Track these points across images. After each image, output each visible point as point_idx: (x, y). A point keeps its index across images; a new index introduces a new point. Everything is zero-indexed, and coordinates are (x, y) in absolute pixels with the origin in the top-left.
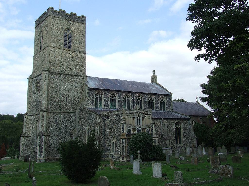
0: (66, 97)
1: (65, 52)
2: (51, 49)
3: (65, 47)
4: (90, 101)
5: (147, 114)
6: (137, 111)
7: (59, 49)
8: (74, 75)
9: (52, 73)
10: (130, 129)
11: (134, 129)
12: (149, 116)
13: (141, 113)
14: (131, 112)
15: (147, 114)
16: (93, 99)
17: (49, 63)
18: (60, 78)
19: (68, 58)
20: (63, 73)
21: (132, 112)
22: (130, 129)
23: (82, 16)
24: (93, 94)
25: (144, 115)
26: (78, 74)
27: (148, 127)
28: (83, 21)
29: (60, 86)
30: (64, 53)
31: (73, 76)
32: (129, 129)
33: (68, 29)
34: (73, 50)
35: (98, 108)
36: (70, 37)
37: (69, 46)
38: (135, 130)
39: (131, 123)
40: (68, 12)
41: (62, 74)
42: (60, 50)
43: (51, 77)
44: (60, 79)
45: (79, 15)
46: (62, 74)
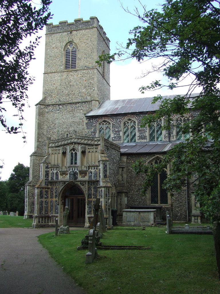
0: (67, 134)
1: (66, 75)
3: (67, 67)
5: (92, 145)
6: (72, 141)
7: (58, 73)
8: (78, 103)
9: (49, 105)
10: (57, 173)
11: (63, 173)
13: (79, 144)
14: (60, 144)
15: (92, 145)
17: (45, 94)
18: (58, 110)
19: (70, 82)
21: (63, 143)
22: (57, 173)
23: (92, 18)
24: (95, 125)
25: (85, 148)
26: (83, 100)
28: (91, 25)
30: (65, 76)
31: (76, 104)
32: (55, 172)
33: (70, 43)
34: (78, 69)
35: (155, 141)
36: (74, 52)
38: (67, 174)
40: (71, 21)
41: (60, 104)
42: (60, 74)
43: (47, 111)
44: (58, 111)
45: (86, 18)
46: (60, 104)
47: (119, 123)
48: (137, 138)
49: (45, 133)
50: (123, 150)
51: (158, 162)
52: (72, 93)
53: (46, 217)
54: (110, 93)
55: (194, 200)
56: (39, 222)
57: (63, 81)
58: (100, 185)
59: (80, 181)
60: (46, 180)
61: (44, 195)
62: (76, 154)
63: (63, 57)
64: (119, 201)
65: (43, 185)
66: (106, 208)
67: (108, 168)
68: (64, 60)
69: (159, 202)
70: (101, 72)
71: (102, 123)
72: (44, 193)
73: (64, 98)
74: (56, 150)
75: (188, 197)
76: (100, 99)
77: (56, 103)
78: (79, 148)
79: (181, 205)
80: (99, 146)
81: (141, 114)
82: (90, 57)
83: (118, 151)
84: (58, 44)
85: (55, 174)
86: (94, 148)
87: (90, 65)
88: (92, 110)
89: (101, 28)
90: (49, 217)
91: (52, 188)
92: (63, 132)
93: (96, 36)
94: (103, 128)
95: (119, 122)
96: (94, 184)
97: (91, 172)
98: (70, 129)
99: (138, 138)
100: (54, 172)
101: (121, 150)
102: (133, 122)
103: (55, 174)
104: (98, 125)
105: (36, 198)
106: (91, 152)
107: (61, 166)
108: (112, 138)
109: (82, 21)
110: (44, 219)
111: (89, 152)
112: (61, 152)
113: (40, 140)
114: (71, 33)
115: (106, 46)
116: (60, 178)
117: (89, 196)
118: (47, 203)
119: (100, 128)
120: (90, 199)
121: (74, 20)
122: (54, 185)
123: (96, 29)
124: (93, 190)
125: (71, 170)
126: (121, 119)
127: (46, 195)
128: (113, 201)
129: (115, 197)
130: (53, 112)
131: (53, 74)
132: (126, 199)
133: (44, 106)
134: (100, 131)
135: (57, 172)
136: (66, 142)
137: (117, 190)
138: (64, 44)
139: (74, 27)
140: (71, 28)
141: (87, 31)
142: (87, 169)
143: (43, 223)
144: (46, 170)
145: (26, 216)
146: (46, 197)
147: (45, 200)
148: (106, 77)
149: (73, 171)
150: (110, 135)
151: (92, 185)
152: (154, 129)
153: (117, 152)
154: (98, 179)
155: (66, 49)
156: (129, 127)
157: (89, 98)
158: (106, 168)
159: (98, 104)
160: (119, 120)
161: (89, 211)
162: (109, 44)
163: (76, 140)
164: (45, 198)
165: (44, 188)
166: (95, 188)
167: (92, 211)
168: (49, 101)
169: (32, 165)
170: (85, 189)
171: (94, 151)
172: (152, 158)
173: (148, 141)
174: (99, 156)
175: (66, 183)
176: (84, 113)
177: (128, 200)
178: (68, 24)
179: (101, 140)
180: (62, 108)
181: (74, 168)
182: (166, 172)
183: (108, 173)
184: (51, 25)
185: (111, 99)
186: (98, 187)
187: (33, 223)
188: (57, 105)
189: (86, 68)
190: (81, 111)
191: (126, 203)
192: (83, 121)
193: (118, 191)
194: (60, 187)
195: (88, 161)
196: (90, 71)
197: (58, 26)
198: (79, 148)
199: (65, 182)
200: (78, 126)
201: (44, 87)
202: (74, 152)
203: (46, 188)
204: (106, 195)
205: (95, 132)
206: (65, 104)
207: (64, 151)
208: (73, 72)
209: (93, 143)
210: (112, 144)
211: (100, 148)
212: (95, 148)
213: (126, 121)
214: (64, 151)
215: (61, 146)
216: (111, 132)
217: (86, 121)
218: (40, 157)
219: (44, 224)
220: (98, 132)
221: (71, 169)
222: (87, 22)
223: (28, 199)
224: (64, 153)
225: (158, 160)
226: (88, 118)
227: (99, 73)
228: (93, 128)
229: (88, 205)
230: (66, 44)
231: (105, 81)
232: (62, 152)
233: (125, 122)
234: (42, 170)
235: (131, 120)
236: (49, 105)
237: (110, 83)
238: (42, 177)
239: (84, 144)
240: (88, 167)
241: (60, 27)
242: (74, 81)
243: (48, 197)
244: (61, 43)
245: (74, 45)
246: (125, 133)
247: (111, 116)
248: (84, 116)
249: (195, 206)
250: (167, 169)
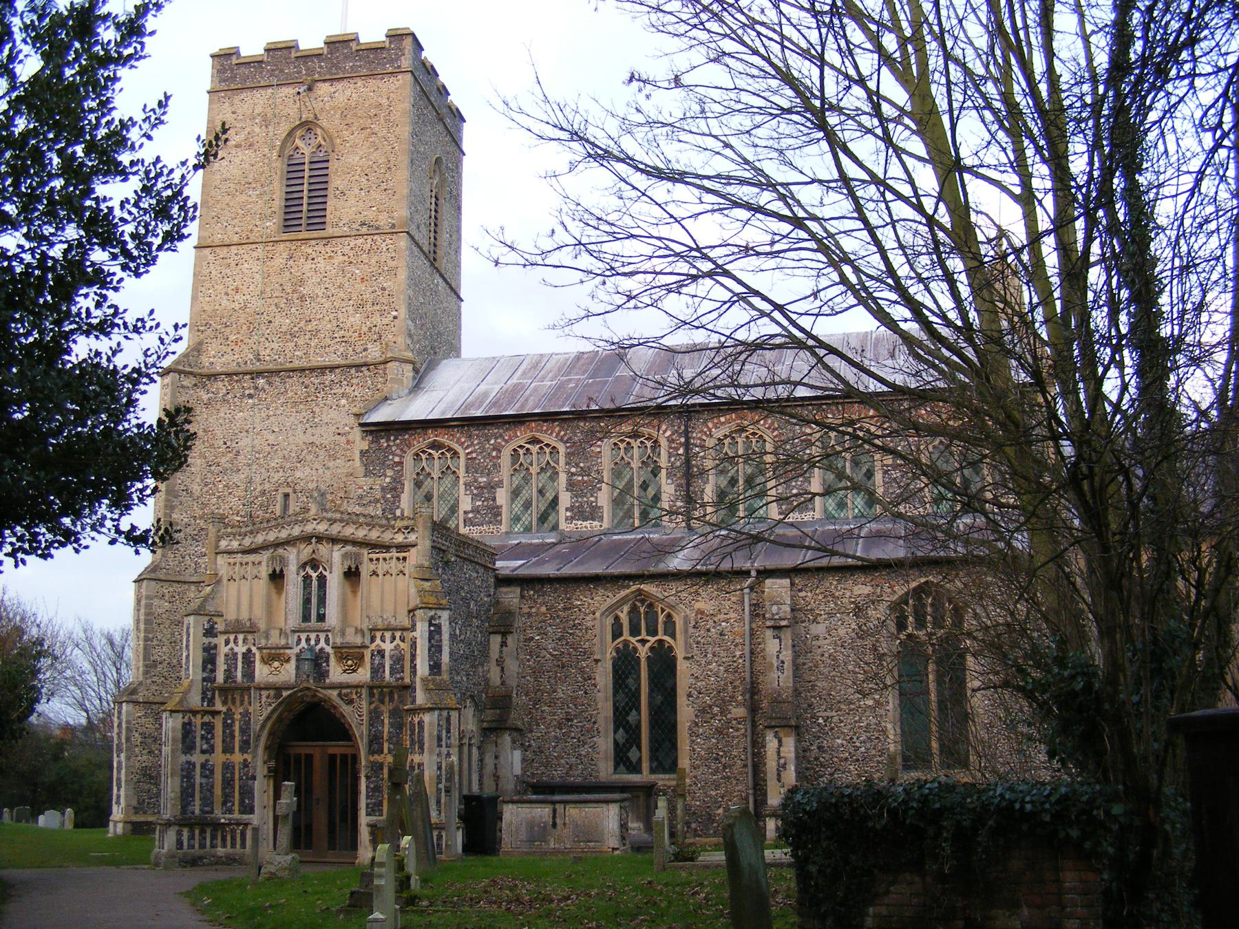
0: (287, 496)
1: (285, 255)
2: (211, 257)
3: (289, 223)
4: (377, 501)
5: (387, 548)
6: (309, 528)
8: (332, 368)
10: (248, 657)
11: (274, 656)
12: (401, 555)
13: (334, 540)
14: (260, 539)
15: (387, 548)
16: (395, 489)
18: (251, 396)
19: (302, 282)
20: (271, 367)
21: (272, 536)
22: (248, 657)
23: (397, 36)
24: (397, 459)
25: (357, 557)
27: (241, 637)
28: (391, 61)
29: (249, 440)
31: (323, 374)
32: (241, 649)
33: (308, 126)
36: (321, 166)
37: (316, 214)
38: (288, 661)
39: (259, 613)
40: (311, 41)
42: (260, 251)
43: (205, 397)
45: (372, 33)
46: (260, 374)
47: (494, 454)
48: (563, 513)
49: (196, 488)
50: (505, 566)
51: (642, 610)
52: (309, 328)
53: (208, 825)
54: (459, 328)
55: (776, 757)
56: (180, 844)
57: (273, 279)
58: (414, 701)
59: (340, 686)
60: (204, 680)
61: (198, 739)
62: (322, 580)
63: (276, 184)
64: (489, 760)
65: (195, 700)
66: (439, 790)
67: (446, 636)
68: (278, 191)
69: (645, 765)
70: (427, 243)
71: (424, 452)
72: (199, 732)
73: (275, 346)
74: (247, 564)
75: (754, 743)
76: (420, 352)
77: (243, 368)
78: (336, 558)
79: (729, 778)
80: (413, 550)
81: (579, 419)
82: (384, 186)
83: (486, 567)
84: (257, 130)
85: (240, 657)
86: (391, 558)
87: (384, 221)
88: (386, 399)
89: (431, 72)
90: (216, 826)
91: (229, 714)
92: (267, 486)
93: (407, 105)
94: (429, 474)
95: (494, 449)
96: (392, 700)
97: (381, 653)
98: (298, 474)
99: (569, 514)
100: (236, 649)
101: (499, 564)
102: (547, 450)
103: (240, 657)
104: (409, 459)
105: (167, 750)
106: (380, 572)
107: (262, 626)
108: (465, 512)
109: (354, 46)
110: (197, 832)
111: (375, 573)
112: (264, 571)
113: (174, 516)
114: (310, 89)
115: (448, 138)
116: (262, 672)
117: (375, 743)
118: (207, 770)
119: (418, 474)
120: (376, 757)
121: (324, 38)
122: (238, 702)
123: (409, 77)
124: (386, 721)
125: (303, 644)
126: (501, 436)
127: (207, 739)
128: (466, 765)
129: (475, 751)
130: (228, 401)
131: (234, 249)
132: (517, 755)
133: (192, 380)
134: (418, 484)
135: (249, 650)
136: (284, 534)
137: (483, 721)
138: (284, 129)
139: (321, 67)
140: (310, 71)
141: (373, 83)
142: (367, 642)
143: (193, 847)
144: (206, 640)
145: (120, 826)
146: (205, 747)
147: (203, 758)
148: (443, 264)
149: (311, 649)
150: (457, 500)
151: (382, 702)
152: (631, 479)
153: (481, 570)
154: (407, 681)
155: (288, 152)
156: (534, 470)
157: (374, 353)
158: (437, 637)
159: (411, 374)
160: (492, 442)
161: (375, 804)
162: (460, 130)
163: (322, 528)
164: (203, 752)
165: (197, 712)
166: (394, 713)
167: (385, 803)
168: (216, 358)
169: (142, 618)
170: (356, 716)
171: (394, 571)
172: (619, 596)
173: (606, 524)
174: (413, 591)
175: (285, 694)
176: (355, 410)
177: (524, 760)
178: (299, 54)
179: (420, 529)
180: (267, 387)
181: (313, 636)
182: (671, 648)
183: (445, 658)
184: (234, 57)
185: (466, 351)
186: (407, 710)
187: (157, 850)
188: (248, 377)
189: (364, 230)
190: (343, 401)
191: (518, 770)
192: (348, 442)
193: (485, 725)
194: (260, 710)
195: (368, 607)
196: (383, 243)
197: (261, 62)
198: (336, 558)
199: (278, 689)
200: (331, 464)
201: (194, 298)
202: (314, 575)
203: (205, 713)
204: (439, 739)
205: (395, 489)
206: (277, 372)
207: (278, 570)
208: (313, 242)
209: (387, 537)
210: (464, 543)
211: (414, 556)
212: (398, 559)
213: (521, 447)
214: (278, 570)
215: (264, 547)
216: (462, 488)
217: (361, 443)
218: (175, 585)
219: (197, 850)
220: (408, 486)
221: (303, 636)
222: (375, 49)
223: (128, 758)
224: (277, 578)
225: (638, 604)
226: (371, 432)
227: (415, 249)
228: (390, 473)
229: (367, 777)
230: (291, 134)
231: (441, 280)
232: (270, 571)
233: (515, 450)
234: (191, 643)
235: (540, 442)
236: (213, 376)
237: (459, 286)
238: (193, 672)
239: (355, 543)
240: (371, 630)
241: (268, 63)
242: (316, 279)
243: (211, 750)
244: (271, 128)
245: (320, 138)
246: (515, 493)
247: (463, 426)
248: (352, 420)
249: (779, 780)
250: (673, 636)
